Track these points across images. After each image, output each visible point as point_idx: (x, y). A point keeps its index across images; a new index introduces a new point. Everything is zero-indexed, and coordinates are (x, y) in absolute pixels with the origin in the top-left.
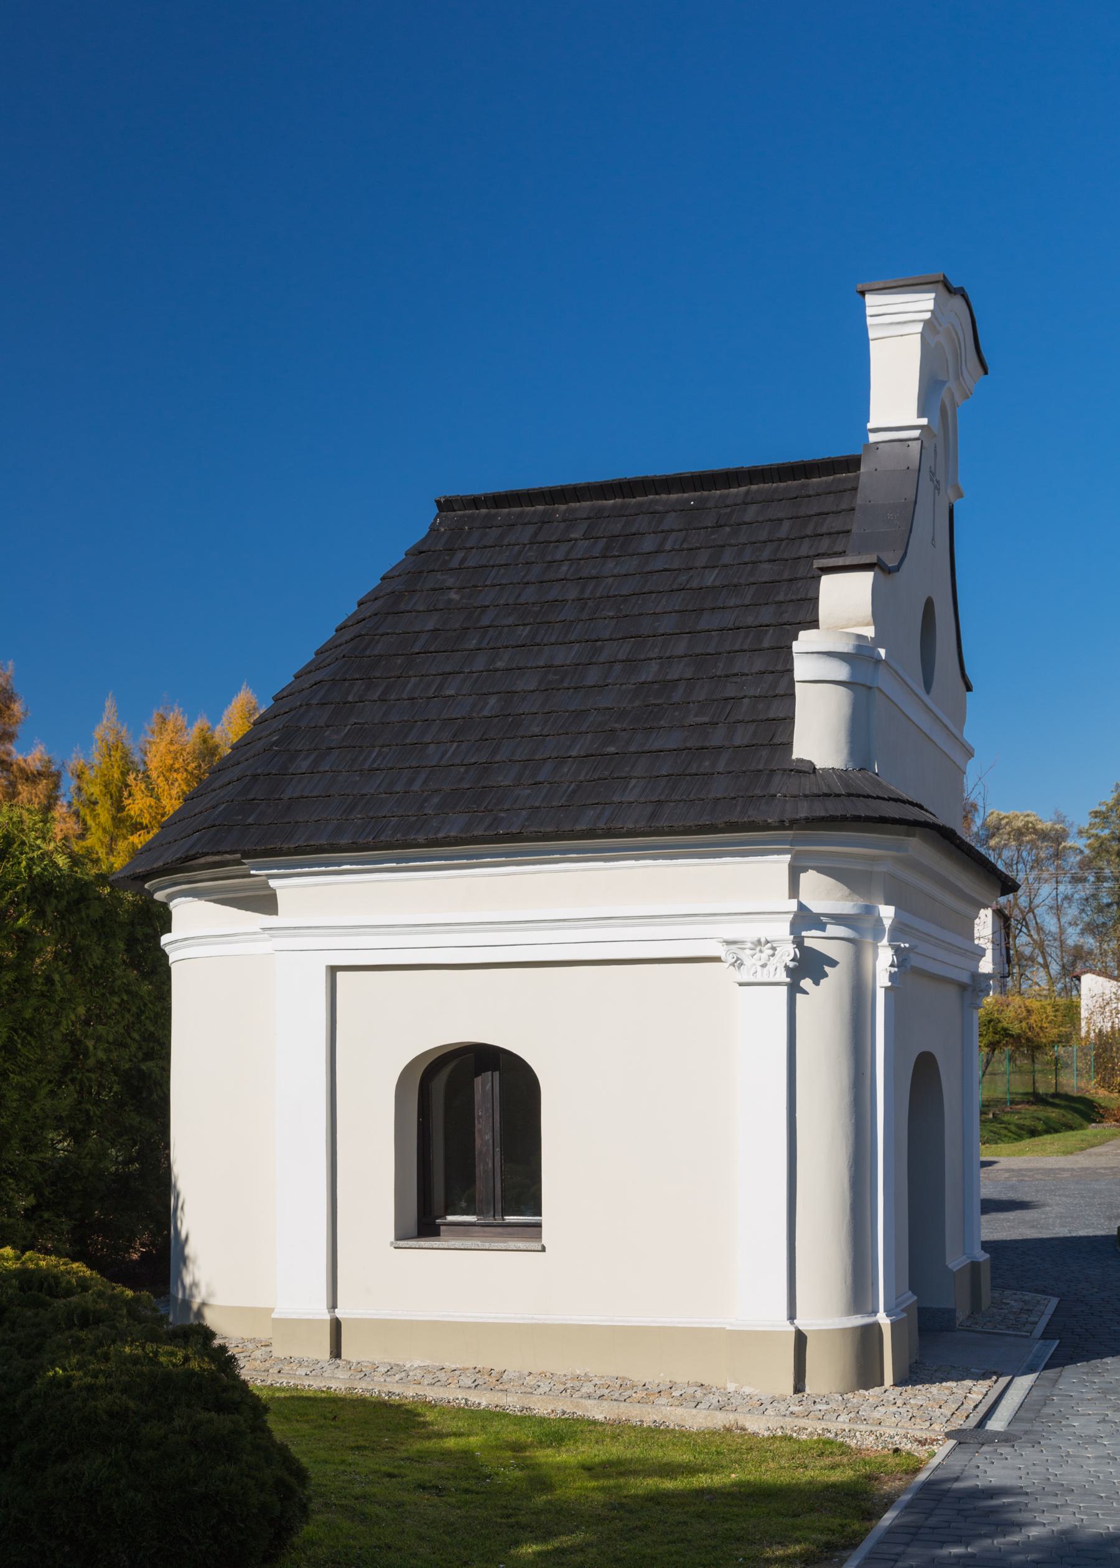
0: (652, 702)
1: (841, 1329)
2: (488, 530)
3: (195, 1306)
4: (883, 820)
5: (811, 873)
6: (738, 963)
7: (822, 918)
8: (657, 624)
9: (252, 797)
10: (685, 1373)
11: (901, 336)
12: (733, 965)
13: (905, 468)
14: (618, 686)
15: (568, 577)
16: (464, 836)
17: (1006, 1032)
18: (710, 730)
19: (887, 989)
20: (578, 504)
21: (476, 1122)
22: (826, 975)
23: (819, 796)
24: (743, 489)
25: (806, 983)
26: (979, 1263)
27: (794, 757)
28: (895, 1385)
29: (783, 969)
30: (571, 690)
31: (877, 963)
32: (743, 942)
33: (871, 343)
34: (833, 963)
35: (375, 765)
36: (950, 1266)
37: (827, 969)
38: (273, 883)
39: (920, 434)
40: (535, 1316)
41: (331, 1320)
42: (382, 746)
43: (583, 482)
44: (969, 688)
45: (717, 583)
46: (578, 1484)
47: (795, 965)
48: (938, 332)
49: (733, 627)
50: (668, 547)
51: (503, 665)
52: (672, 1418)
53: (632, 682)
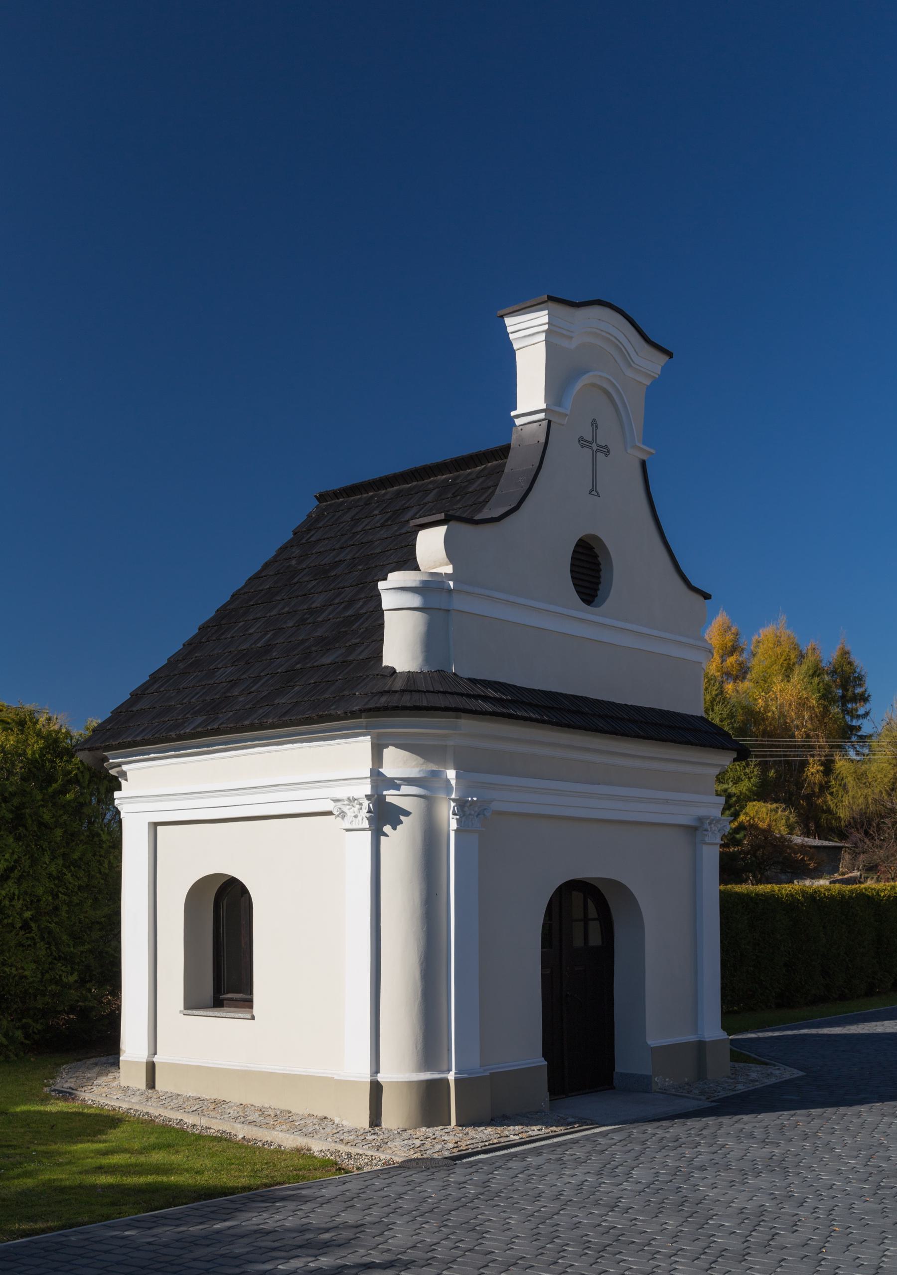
5: (391, 748)
6: (343, 814)
11: (534, 344)
13: (537, 442)
16: (193, 731)
22: (401, 822)
24: (483, 466)
25: (387, 829)
27: (383, 665)
28: (458, 1125)
33: (516, 352)
34: (407, 813)
36: (649, 1042)
37: (402, 818)
38: (125, 768)
39: (545, 415)
40: (249, 1065)
41: (147, 1063)
47: (371, 816)
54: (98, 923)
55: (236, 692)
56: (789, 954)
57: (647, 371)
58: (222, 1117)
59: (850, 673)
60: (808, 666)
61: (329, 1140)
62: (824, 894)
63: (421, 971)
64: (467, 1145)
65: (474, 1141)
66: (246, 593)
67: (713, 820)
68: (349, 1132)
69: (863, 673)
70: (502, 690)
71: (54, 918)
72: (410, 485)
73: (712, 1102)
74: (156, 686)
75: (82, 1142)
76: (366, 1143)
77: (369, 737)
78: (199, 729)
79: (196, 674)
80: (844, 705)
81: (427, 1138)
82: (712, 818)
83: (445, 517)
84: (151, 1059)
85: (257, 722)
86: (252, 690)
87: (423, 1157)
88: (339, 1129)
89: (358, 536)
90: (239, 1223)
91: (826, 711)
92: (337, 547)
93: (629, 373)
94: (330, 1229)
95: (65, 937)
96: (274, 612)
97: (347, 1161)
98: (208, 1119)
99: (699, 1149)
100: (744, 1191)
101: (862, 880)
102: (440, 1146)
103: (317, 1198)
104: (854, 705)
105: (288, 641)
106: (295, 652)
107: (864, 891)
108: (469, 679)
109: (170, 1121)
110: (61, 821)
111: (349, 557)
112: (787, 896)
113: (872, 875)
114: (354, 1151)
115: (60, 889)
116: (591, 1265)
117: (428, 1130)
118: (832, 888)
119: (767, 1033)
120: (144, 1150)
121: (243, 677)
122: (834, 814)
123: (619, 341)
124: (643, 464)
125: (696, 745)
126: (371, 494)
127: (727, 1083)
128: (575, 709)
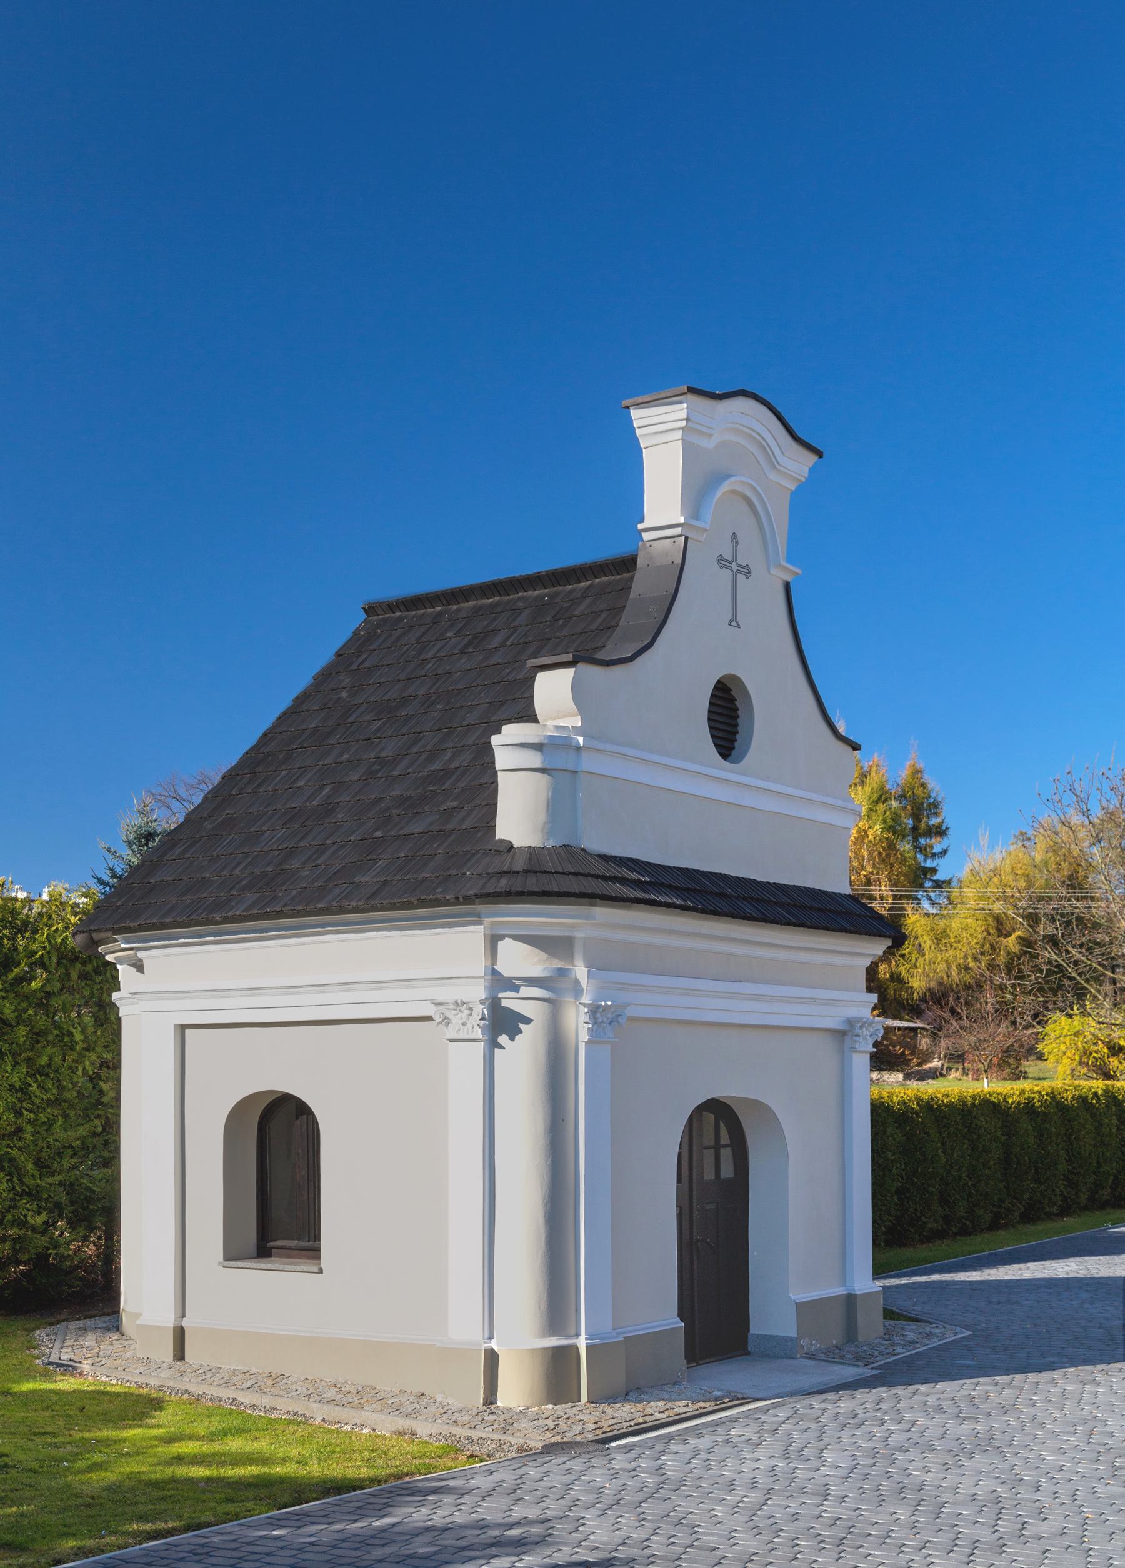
1: (541, 1349)
6: (446, 1021)
7: (514, 981)
12: (441, 1023)
13: (671, 563)
16: (245, 914)
19: (586, 1042)
22: (521, 1032)
24: (589, 583)
25: (503, 1039)
26: (856, 1295)
28: (590, 1401)
34: (528, 1021)
37: (521, 1026)
41: (174, 1327)
45: (527, 676)
49: (517, 716)
50: (508, 643)
54: (71, 1147)
55: (295, 864)
56: (902, 1178)
57: (792, 473)
58: (290, 1395)
59: (923, 798)
60: (872, 789)
61: (439, 1421)
62: (943, 1101)
63: (545, 1213)
64: (610, 1426)
65: (615, 1421)
67: (865, 1023)
68: (460, 1411)
69: (939, 799)
70: (641, 872)
71: (16, 1142)
72: (491, 600)
73: (872, 1368)
74: (178, 851)
75: (131, 1427)
76: (487, 1425)
78: (255, 911)
79: (231, 837)
80: (916, 839)
81: (559, 1418)
82: (864, 1020)
83: (573, 658)
84: (178, 1323)
85: (336, 905)
86: (319, 862)
87: (564, 1440)
88: (446, 1408)
89: (430, 665)
90: (400, 1520)
91: (891, 846)
92: (402, 676)
93: (773, 476)
94: (514, 1525)
95: (30, 1166)
96: (329, 760)
97: (470, 1446)
98: (286, 1400)
99: (886, 1426)
100: (964, 1474)
101: (944, 1072)
102: (580, 1428)
103: (473, 1490)
104: (928, 840)
105: (356, 799)
106: (370, 815)
107: (988, 1096)
108: (600, 856)
109: (220, 1401)
110: (25, 1016)
111: (422, 692)
112: (898, 1104)
113: (956, 1066)
114: (475, 1434)
115: (24, 1104)
116: (837, 1560)
117: (556, 1407)
118: (950, 1093)
119: (893, 1280)
120: (211, 1437)
121: (302, 844)
122: (905, 983)
123: (763, 438)
124: (787, 587)
125: (851, 932)
126: (439, 609)
127: (883, 1345)
128: (718, 891)
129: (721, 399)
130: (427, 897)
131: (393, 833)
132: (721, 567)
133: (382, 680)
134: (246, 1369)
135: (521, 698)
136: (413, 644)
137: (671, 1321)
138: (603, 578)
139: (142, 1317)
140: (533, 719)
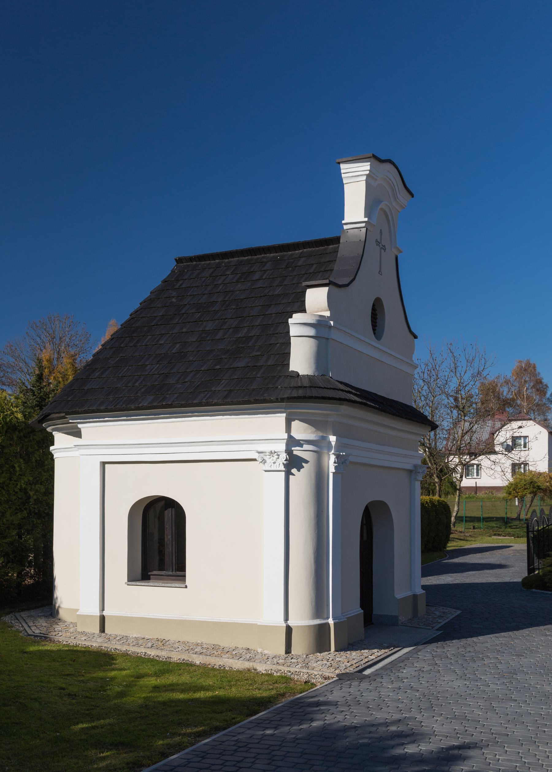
0: (240, 346)
1: (313, 625)
2: (194, 271)
3: (57, 607)
4: (324, 398)
6: (264, 461)
8: (251, 311)
9: (73, 388)
10: (242, 644)
12: (261, 462)
14: (229, 339)
15: (221, 291)
16: (150, 405)
17: (539, 488)
18: (260, 358)
19: (334, 473)
20: (233, 259)
21: (165, 530)
22: (303, 467)
23: (297, 387)
24: (301, 251)
25: (294, 471)
26: (417, 595)
27: (290, 370)
28: (336, 651)
29: (282, 464)
30: (210, 341)
31: (330, 461)
32: (265, 452)
33: (345, 185)
34: (307, 462)
35: (124, 375)
36: (396, 597)
37: (304, 464)
39: (365, 225)
40: (183, 616)
41: (100, 616)
42: (129, 366)
43: (234, 249)
44: (415, 337)
45: (280, 293)
46: (138, 695)
47: (287, 463)
48: (376, 180)
49: (281, 312)
50: (264, 277)
51: (186, 330)
52: (228, 664)
53: (235, 337)
55: (172, 381)
66: (144, 317)
72: (247, 258)
77: (285, 414)
78: (155, 404)
93: (394, 204)
96: (175, 331)
108: (336, 381)
109: (138, 654)
117: (322, 654)
129: (383, 162)
130: (260, 398)
131: (226, 367)
132: (377, 245)
133: (195, 294)
134: (143, 636)
135: (280, 304)
136: (208, 277)
137: (355, 610)
138: (309, 249)
139: (79, 611)
140: (303, 310)
